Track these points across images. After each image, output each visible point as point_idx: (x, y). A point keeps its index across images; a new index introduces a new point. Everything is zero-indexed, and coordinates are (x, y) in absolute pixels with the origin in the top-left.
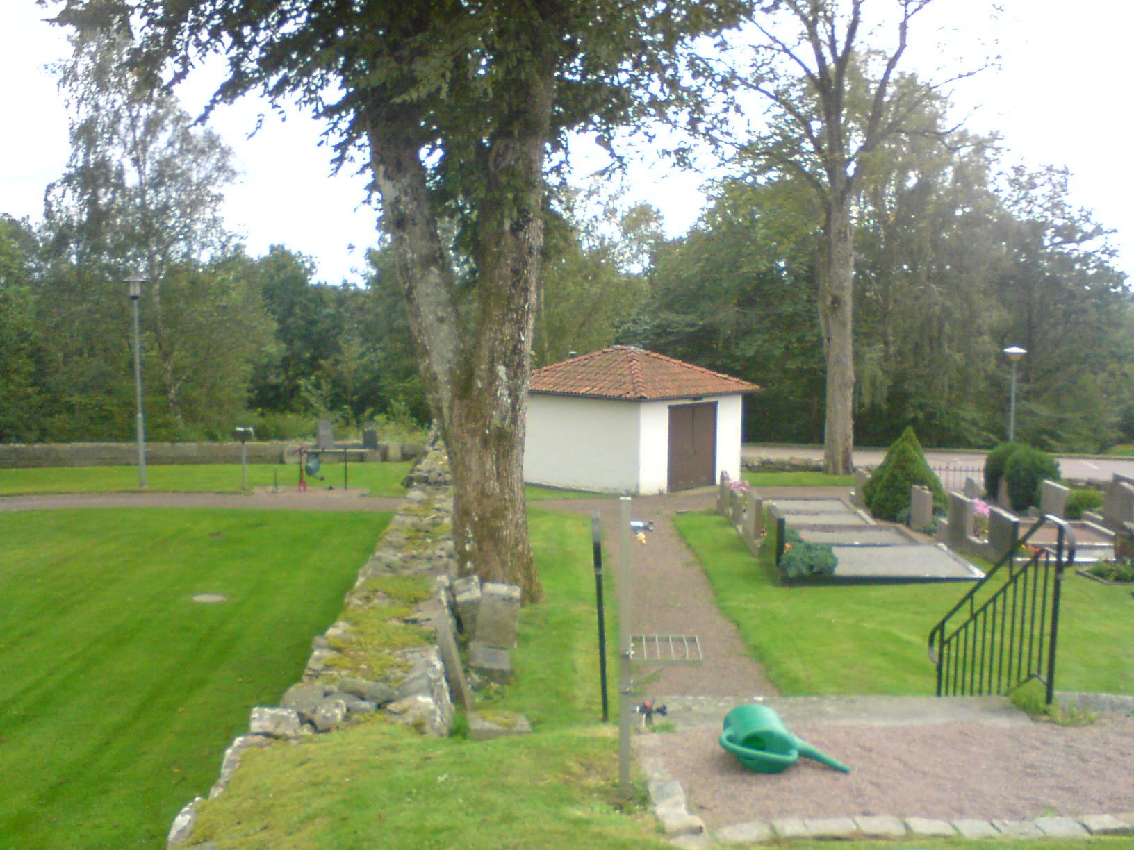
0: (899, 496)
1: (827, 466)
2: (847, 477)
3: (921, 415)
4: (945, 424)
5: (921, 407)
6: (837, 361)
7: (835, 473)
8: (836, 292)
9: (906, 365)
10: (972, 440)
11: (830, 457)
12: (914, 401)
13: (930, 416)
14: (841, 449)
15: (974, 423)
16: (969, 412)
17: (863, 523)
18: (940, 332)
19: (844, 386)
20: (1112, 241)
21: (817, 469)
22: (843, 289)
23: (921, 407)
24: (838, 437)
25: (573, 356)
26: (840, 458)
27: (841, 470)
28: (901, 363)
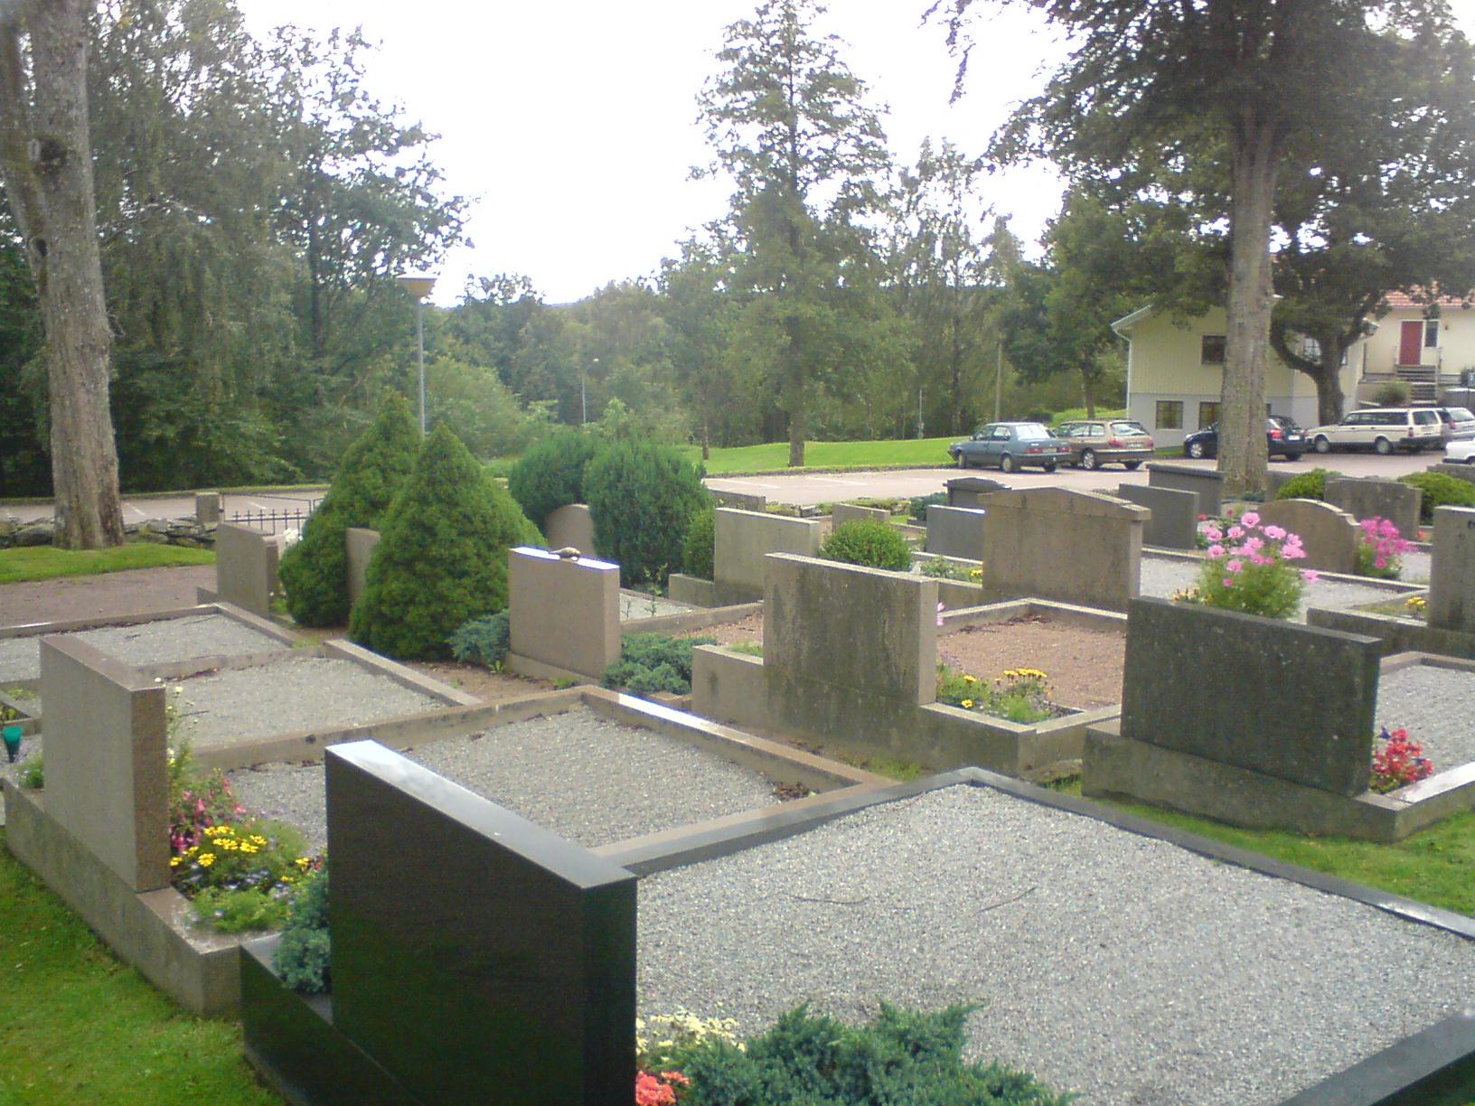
0: (445, 584)
1: (66, 532)
2: (115, 550)
3: (171, 432)
4: (215, 446)
5: (169, 418)
6: (69, 294)
7: (87, 544)
8: (49, 131)
9: (142, 344)
10: (255, 471)
11: (73, 512)
12: (160, 408)
13: (188, 434)
14: (96, 490)
15: (262, 441)
16: (255, 423)
17: (443, 709)
18: (199, 285)
19: (87, 350)
20: (435, 154)
21: (40, 539)
22: (70, 124)
23: (169, 418)
24: (87, 463)
25: (286, 883)
26: (95, 512)
27: (99, 537)
28: (129, 342)
